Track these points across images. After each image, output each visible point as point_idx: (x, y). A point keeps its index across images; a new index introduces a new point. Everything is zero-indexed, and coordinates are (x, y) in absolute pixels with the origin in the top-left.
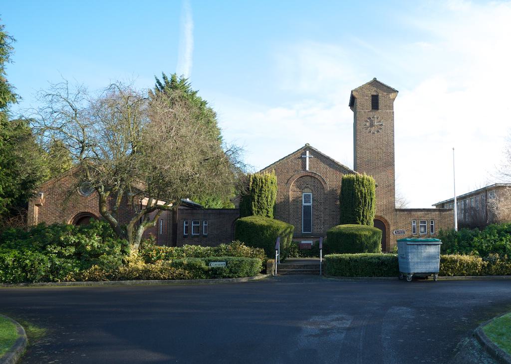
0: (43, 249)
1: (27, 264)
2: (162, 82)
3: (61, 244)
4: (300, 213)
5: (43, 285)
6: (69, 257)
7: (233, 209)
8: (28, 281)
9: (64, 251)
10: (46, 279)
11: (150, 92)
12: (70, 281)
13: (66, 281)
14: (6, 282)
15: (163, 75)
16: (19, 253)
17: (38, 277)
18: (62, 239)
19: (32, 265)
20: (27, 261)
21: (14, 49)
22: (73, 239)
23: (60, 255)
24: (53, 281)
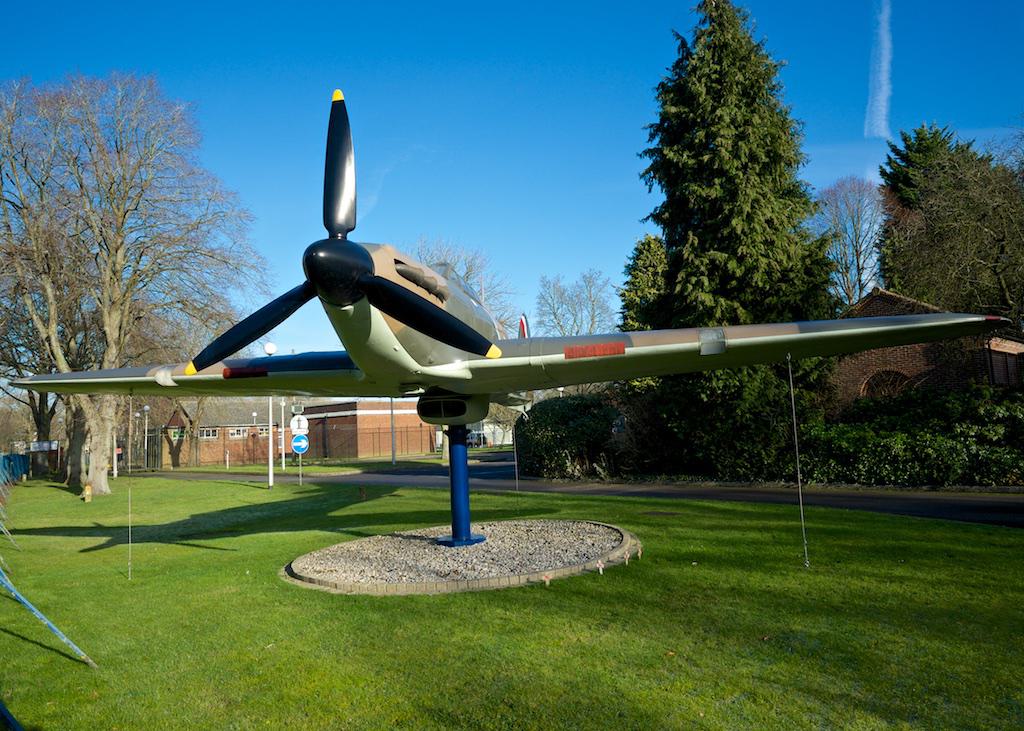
0: (947, 430)
1: (928, 455)
2: (901, 146)
3: (979, 421)
4: (603, 519)
5: (963, 491)
6: (998, 443)
7: (468, 506)
8: (935, 484)
9: (987, 433)
10: (966, 480)
11: (975, 154)
12: (1015, 484)
13: (1007, 484)
14: (898, 484)
15: (902, 134)
16: (907, 438)
17: (952, 477)
18: (982, 412)
19: (938, 457)
20: (930, 451)
21: (638, 155)
22: (1001, 412)
23: (981, 440)
24: (980, 484)
